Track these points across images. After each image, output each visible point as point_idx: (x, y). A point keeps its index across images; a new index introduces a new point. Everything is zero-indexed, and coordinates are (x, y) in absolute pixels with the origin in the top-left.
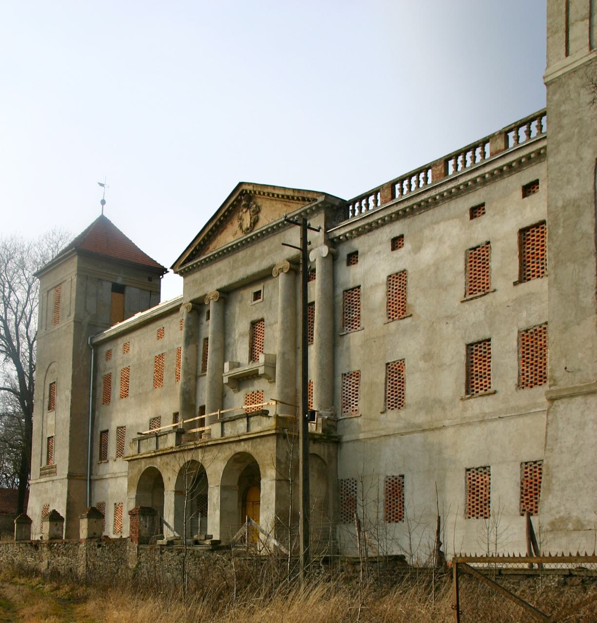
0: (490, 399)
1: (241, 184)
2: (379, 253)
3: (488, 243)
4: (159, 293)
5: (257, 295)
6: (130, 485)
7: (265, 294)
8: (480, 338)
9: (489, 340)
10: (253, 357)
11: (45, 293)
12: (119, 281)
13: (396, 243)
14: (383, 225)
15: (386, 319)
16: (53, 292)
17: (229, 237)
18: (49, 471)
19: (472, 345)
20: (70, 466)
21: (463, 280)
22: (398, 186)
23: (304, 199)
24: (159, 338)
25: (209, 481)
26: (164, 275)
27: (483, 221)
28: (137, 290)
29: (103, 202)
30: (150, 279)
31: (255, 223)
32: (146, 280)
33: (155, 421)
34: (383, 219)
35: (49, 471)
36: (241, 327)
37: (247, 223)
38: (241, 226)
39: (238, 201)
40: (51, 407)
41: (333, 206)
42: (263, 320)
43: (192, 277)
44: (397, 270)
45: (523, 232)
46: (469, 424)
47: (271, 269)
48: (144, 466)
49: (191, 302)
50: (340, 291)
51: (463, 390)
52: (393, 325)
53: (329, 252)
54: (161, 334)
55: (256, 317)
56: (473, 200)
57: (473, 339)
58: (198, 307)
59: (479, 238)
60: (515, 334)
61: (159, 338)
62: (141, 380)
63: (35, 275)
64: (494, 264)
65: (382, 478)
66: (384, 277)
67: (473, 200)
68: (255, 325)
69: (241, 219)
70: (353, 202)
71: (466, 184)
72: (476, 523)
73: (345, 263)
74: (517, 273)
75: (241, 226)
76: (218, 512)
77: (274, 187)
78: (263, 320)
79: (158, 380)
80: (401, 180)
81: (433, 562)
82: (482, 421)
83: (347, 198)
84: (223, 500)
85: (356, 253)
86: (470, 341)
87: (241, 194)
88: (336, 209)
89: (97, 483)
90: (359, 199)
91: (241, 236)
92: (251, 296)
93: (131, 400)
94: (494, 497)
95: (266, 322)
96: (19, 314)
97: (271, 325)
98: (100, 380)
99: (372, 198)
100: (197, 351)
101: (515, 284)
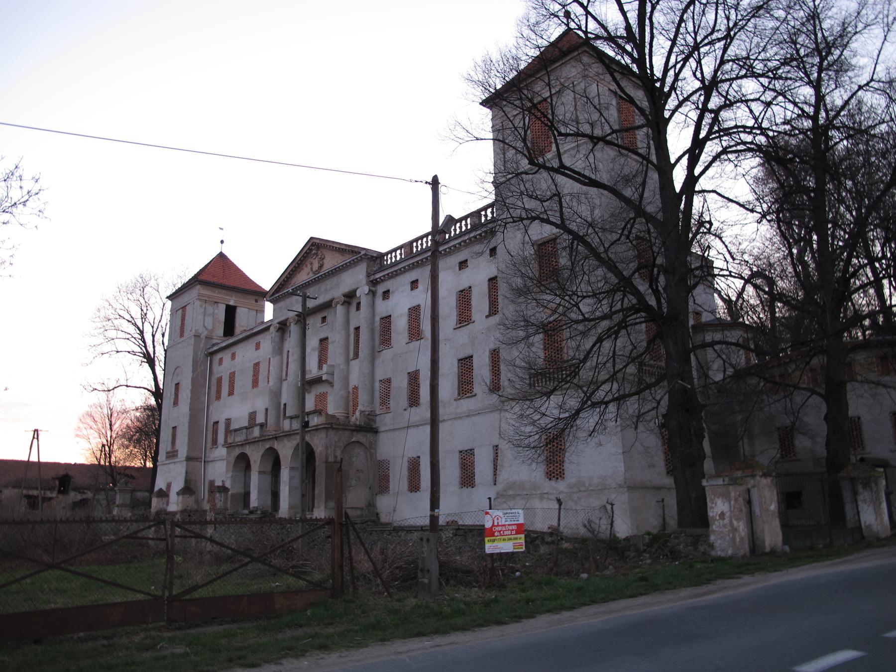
0: (473, 399)
1: (311, 238)
2: (402, 292)
3: (470, 287)
4: (263, 311)
5: (324, 319)
6: (227, 466)
7: (329, 319)
8: (466, 355)
9: (472, 357)
10: (320, 367)
11: (173, 312)
12: (232, 303)
13: (463, 264)
14: (405, 272)
15: (407, 340)
16: (180, 311)
17: (303, 277)
18: (172, 455)
19: (461, 360)
20: (188, 451)
21: (455, 314)
22: (415, 244)
23: (353, 252)
24: (257, 349)
25: (282, 463)
26: (428, 228)
27: (467, 272)
28: (246, 310)
29: (222, 242)
30: (256, 301)
31: (321, 266)
32: (254, 302)
33: (252, 416)
34: (404, 268)
35: (172, 455)
36: (312, 343)
37: (316, 266)
38: (312, 269)
39: (310, 250)
40: (176, 403)
41: (372, 257)
42: (327, 338)
43: (281, 304)
44: (414, 305)
45: (490, 280)
46: (460, 418)
47: (331, 301)
48: (237, 452)
49: (279, 323)
50: (377, 319)
51: (456, 393)
52: (412, 345)
53: (370, 290)
54: (258, 347)
55: (323, 336)
56: (461, 257)
57: (462, 356)
58: (283, 327)
59: (465, 285)
60: (487, 354)
61: (257, 349)
62: (243, 381)
63: (168, 298)
64: (474, 302)
65: (406, 460)
66: (406, 310)
67: (461, 257)
68: (324, 341)
69: (311, 264)
70: (387, 254)
71: (455, 246)
72: (467, 491)
73: (381, 298)
74: (488, 310)
75: (312, 269)
76: (287, 488)
77: (334, 242)
78: (327, 338)
79: (255, 383)
80: (416, 240)
81: (427, 522)
82: (468, 416)
83: (383, 250)
84: (291, 478)
85: (389, 291)
86: (460, 357)
87: (312, 245)
88: (374, 259)
89: (211, 465)
90: (391, 252)
91: (311, 276)
92: (320, 320)
93: (235, 397)
94: (477, 471)
95: (330, 340)
96: (155, 327)
97: (333, 342)
98: (214, 381)
99: (398, 252)
100: (282, 361)
101: (487, 317)
